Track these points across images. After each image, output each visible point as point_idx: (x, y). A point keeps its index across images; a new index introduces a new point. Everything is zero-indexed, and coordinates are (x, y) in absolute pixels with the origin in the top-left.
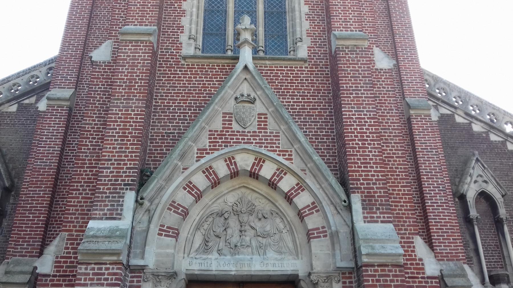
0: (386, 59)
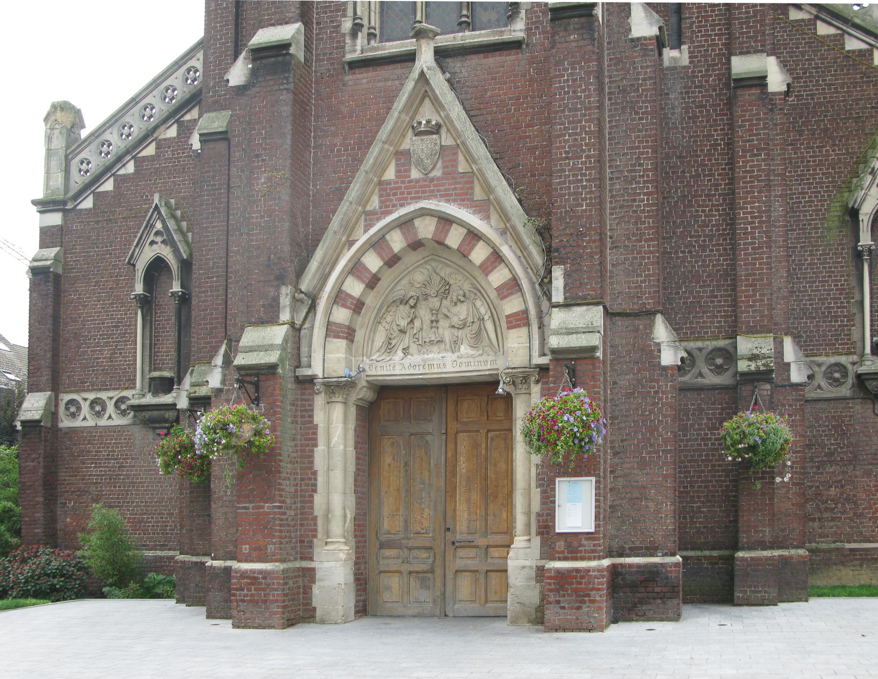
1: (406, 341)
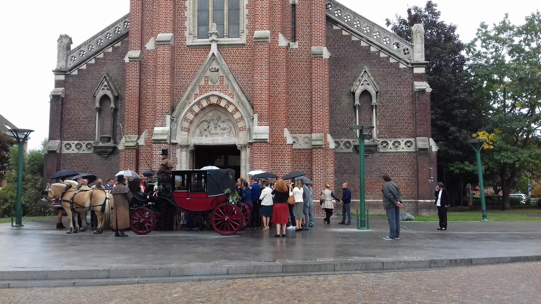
0: (285, 41)
1: (206, 133)
